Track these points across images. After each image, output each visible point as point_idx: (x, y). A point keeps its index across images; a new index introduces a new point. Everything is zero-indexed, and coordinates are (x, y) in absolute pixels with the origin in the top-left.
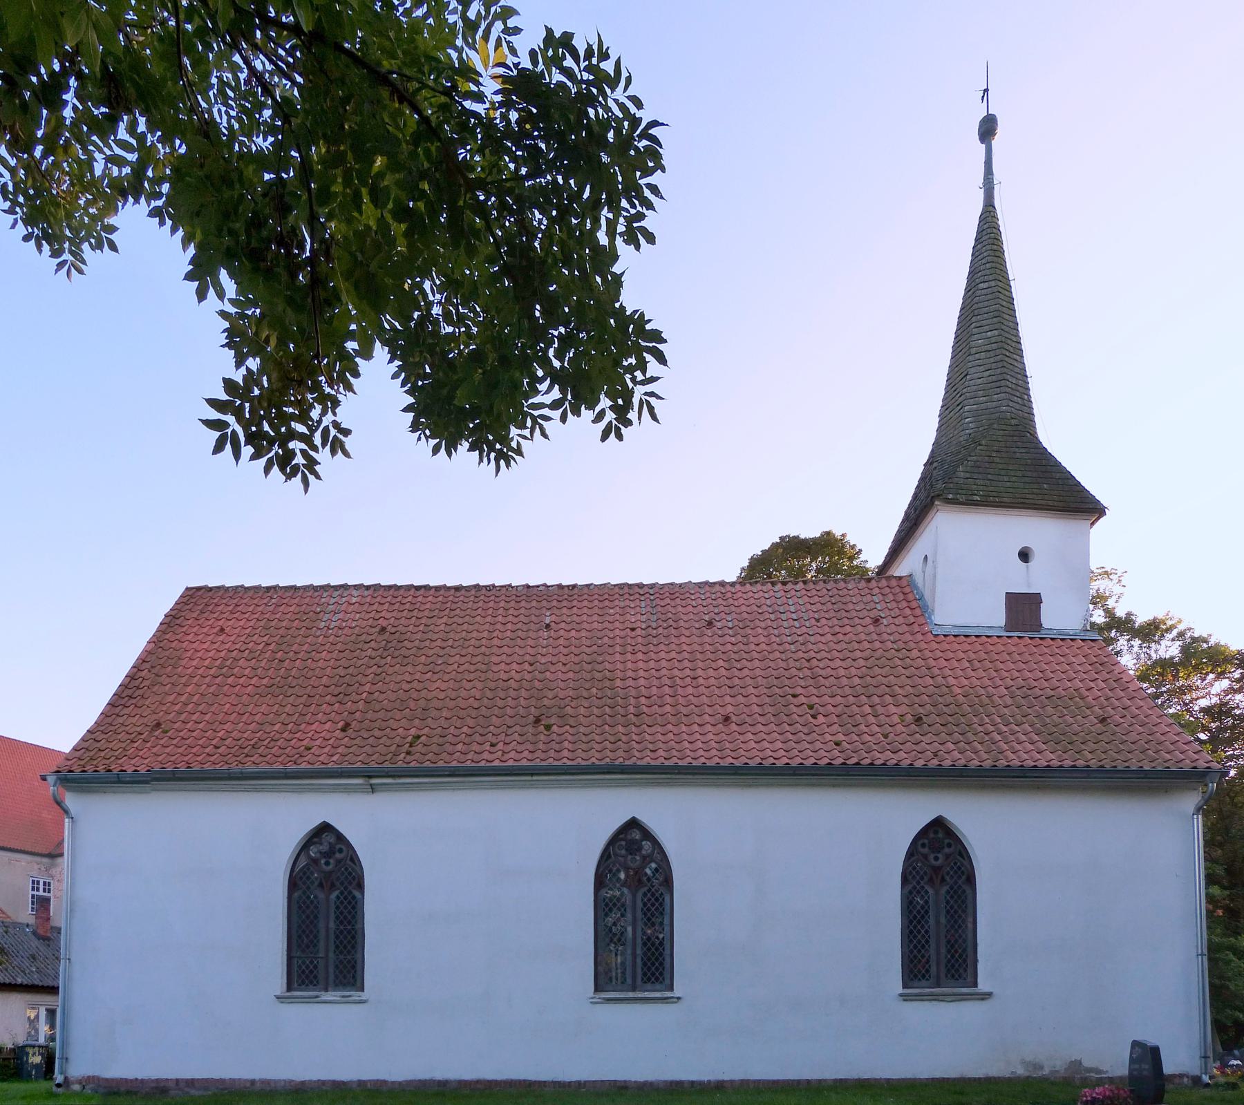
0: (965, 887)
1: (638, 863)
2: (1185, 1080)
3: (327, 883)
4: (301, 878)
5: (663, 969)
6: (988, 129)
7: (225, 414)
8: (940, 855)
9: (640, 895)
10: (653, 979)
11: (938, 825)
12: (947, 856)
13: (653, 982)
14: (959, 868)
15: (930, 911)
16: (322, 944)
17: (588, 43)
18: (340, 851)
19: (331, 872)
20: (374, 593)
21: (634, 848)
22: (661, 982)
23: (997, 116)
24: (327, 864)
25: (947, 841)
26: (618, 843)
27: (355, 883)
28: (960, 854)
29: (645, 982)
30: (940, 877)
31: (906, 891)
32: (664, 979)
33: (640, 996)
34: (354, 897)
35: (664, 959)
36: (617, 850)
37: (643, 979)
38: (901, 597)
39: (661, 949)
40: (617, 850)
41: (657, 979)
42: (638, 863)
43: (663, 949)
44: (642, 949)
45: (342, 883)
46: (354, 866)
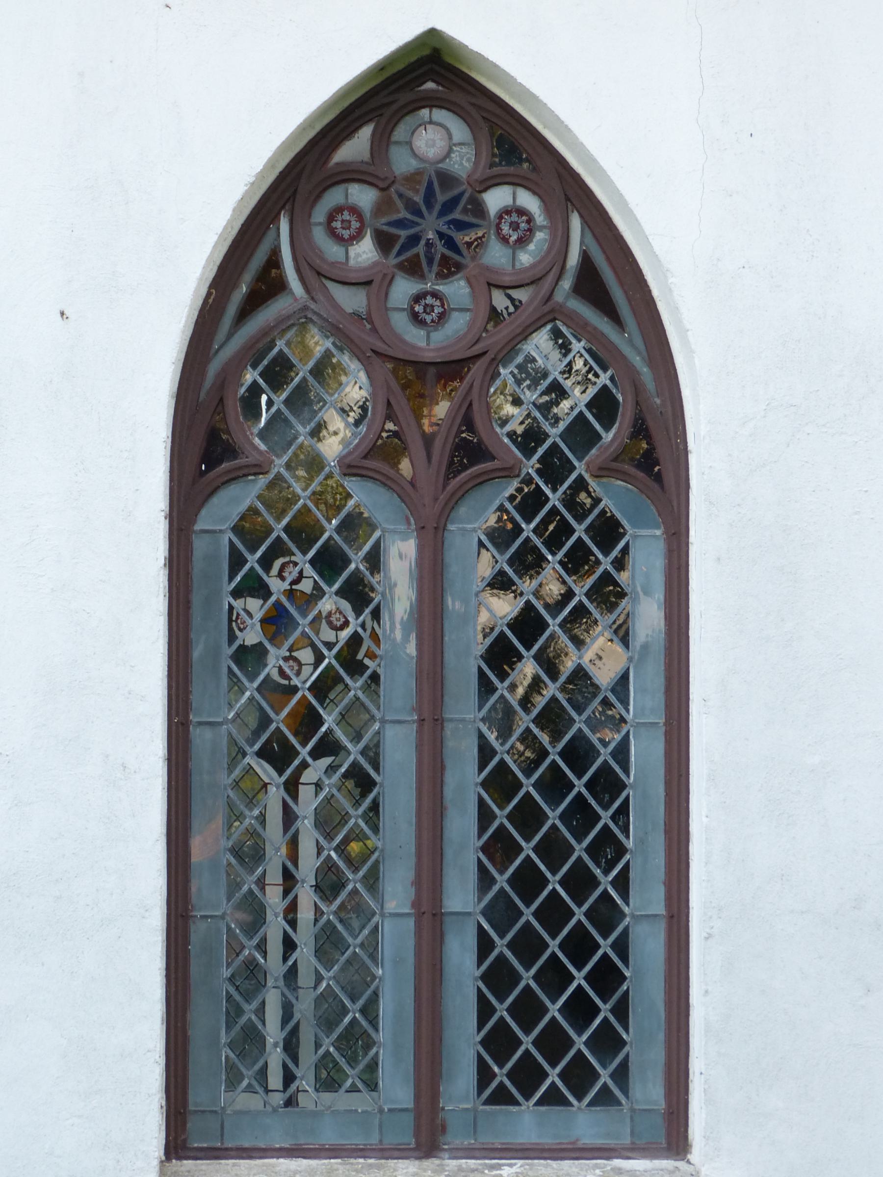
1: (458, 323)
2: (568, 492)
5: (622, 1011)
7: (542, 729)
10: (553, 1076)
13: (553, 1098)
17: (300, 988)
21: (328, 353)
22: (605, 1098)
23: (439, 27)
26: (334, 197)
29: (501, 1097)
32: (622, 1074)
35: (622, 947)
36: (319, 235)
37: (484, 1075)
39: (605, 882)
40: (319, 235)
42: (458, 323)
43: (622, 883)
44: (485, 879)
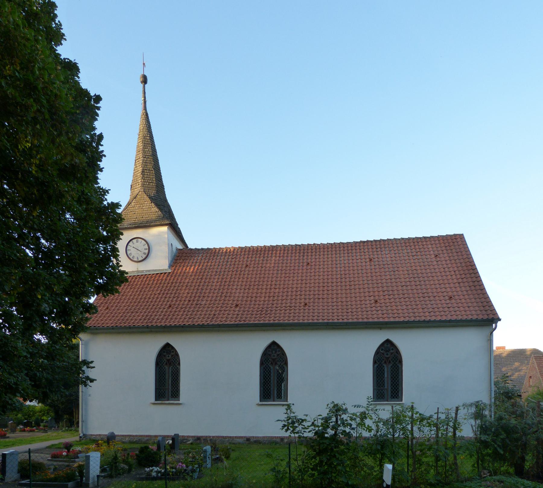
0: (285, 366)
3: (169, 362)
4: (264, 361)
6: (145, 80)
8: (388, 353)
9: (171, 368)
10: (380, 398)
11: (388, 341)
12: (172, 356)
14: (396, 358)
15: (171, 375)
16: (386, 384)
18: (173, 352)
19: (389, 358)
20: (212, 261)
24: (168, 356)
25: (391, 348)
27: (398, 361)
28: (397, 352)
30: (388, 361)
31: (376, 366)
33: (275, 403)
34: (398, 366)
38: (451, 244)
41: (176, 397)
45: (393, 361)
46: (397, 355)
